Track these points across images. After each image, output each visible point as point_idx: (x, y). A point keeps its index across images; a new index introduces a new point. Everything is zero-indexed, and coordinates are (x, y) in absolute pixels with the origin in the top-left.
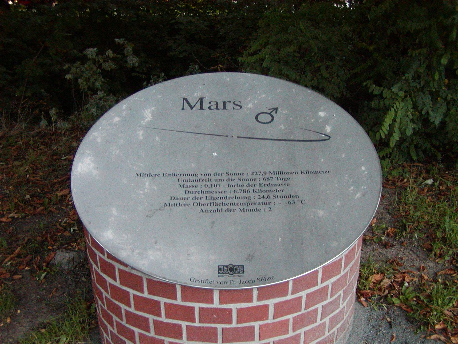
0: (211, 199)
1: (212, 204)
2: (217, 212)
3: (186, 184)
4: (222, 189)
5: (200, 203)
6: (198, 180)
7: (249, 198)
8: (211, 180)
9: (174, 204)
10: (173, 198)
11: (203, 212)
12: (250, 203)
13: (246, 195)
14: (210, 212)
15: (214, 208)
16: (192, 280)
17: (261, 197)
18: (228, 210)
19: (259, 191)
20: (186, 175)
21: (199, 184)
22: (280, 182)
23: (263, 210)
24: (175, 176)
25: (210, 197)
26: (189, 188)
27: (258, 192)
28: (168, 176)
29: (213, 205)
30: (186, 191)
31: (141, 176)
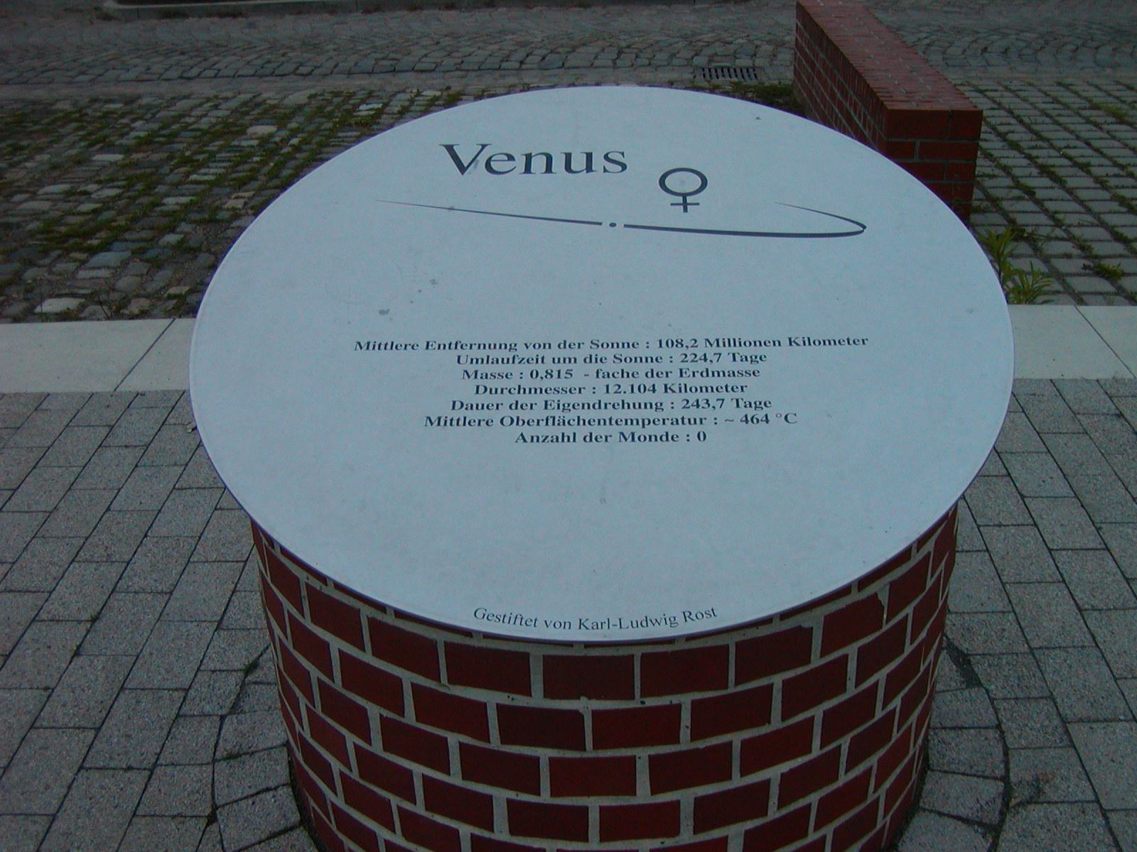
0: (559, 408)
1: (550, 422)
2: (563, 440)
3: (483, 369)
4: (573, 383)
5: (518, 418)
6: (508, 359)
7: (659, 407)
8: (543, 358)
9: (452, 420)
10: (458, 405)
11: (525, 441)
12: (526, 421)
13: (648, 397)
14: (544, 441)
15: (557, 431)
16: (479, 614)
17: (690, 404)
18: (590, 438)
19: (680, 388)
20: (487, 346)
21: (515, 368)
22: (740, 366)
23: (683, 438)
24: (456, 348)
25: (556, 401)
26: (488, 380)
27: (678, 391)
28: (439, 348)
29: (554, 424)
30: (478, 387)
31: (368, 348)
